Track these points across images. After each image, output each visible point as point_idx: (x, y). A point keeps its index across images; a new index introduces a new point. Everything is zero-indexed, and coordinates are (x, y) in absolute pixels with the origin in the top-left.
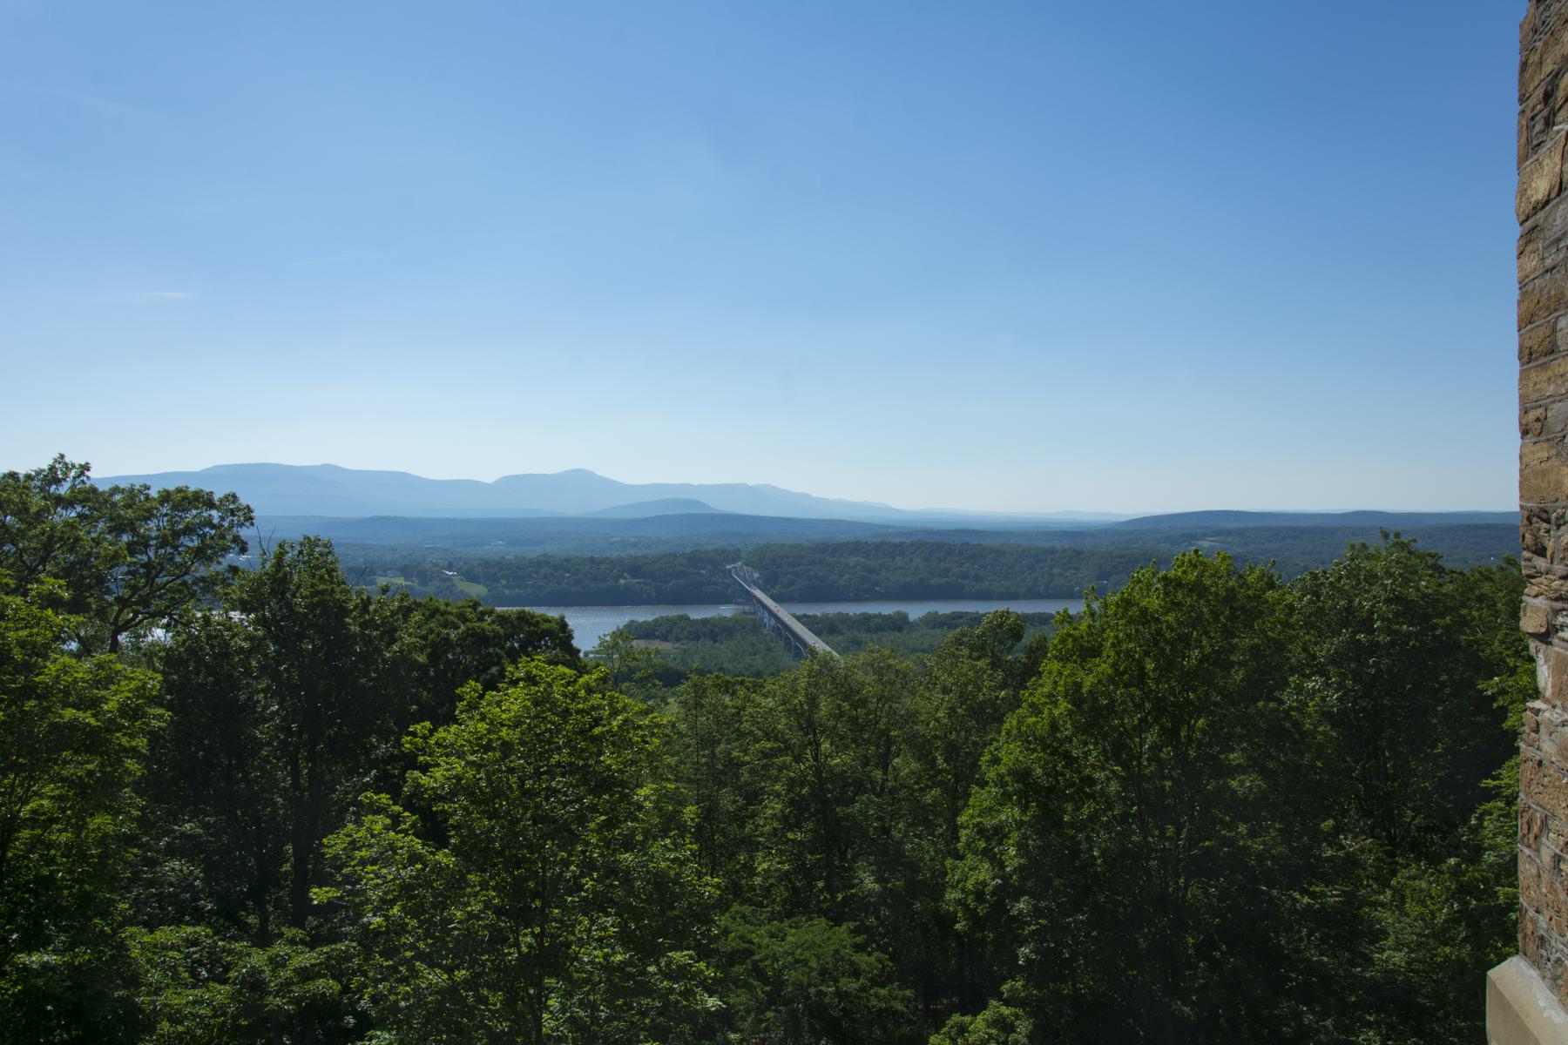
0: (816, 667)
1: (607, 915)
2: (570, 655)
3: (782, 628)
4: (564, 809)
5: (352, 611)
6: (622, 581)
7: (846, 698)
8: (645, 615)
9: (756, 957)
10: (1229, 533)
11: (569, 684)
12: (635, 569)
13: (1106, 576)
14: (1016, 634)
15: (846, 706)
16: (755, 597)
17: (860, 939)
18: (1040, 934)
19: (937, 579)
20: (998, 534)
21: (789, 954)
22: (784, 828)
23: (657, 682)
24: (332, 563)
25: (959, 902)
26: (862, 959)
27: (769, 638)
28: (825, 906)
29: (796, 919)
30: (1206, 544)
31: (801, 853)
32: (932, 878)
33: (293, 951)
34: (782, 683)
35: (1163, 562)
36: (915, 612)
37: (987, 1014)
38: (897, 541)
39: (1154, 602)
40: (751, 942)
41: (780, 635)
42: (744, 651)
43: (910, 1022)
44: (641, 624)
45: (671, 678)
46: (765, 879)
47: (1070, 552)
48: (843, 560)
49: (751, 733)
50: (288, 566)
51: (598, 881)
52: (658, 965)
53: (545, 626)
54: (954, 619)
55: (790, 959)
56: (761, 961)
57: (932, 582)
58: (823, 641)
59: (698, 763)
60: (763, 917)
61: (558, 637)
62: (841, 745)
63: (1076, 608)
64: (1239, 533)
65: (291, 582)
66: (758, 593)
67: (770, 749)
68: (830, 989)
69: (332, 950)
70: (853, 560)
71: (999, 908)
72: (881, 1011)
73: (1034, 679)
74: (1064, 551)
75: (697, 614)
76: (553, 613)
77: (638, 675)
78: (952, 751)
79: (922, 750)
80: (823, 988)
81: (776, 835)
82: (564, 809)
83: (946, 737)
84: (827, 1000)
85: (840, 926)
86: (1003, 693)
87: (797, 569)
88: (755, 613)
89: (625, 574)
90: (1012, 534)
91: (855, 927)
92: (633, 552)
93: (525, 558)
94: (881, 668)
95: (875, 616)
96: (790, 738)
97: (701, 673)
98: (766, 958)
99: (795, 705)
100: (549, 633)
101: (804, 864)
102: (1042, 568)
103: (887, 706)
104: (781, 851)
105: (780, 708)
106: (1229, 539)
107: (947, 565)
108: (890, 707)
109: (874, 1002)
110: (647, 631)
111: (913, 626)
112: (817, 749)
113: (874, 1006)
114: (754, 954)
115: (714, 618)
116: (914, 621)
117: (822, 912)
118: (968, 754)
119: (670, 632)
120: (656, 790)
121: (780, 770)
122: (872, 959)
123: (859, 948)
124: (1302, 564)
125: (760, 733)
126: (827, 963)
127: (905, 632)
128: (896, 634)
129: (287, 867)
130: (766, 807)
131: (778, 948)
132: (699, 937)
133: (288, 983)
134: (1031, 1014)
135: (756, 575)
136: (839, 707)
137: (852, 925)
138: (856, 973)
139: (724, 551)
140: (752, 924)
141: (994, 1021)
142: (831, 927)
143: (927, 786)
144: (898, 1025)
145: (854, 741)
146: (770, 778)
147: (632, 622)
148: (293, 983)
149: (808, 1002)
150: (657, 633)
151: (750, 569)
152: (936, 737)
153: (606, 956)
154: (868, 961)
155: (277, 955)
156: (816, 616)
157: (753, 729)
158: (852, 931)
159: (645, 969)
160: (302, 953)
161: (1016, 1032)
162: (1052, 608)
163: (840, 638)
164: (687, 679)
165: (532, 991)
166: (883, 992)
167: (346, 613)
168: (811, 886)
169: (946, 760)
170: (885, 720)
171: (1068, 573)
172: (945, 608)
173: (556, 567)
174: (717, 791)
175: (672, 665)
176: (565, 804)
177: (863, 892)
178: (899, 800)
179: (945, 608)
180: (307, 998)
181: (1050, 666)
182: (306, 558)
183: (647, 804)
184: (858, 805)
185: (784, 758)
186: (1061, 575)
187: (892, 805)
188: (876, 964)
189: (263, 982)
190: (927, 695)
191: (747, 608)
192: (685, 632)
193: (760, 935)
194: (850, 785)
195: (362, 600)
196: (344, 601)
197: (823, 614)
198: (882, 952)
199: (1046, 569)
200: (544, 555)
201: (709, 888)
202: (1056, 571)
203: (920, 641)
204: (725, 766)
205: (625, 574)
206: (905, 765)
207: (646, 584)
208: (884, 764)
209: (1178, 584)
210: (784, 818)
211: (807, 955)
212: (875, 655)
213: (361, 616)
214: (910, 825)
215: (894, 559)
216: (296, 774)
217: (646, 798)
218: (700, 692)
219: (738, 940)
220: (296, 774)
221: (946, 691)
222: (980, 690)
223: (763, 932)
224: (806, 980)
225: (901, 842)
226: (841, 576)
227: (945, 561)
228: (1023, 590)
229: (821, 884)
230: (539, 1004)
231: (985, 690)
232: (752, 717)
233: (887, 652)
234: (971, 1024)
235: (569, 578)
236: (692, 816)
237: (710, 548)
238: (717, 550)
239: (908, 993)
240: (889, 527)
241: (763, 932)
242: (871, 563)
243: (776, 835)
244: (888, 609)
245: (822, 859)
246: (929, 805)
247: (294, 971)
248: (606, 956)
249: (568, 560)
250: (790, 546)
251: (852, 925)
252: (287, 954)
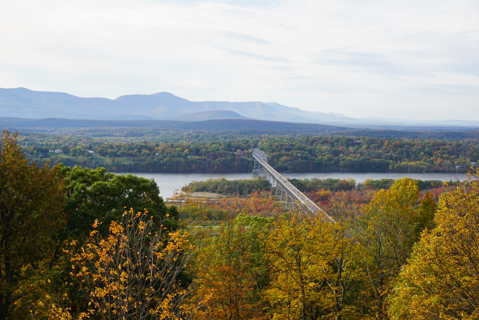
36: (360, 179)
110: (203, 188)
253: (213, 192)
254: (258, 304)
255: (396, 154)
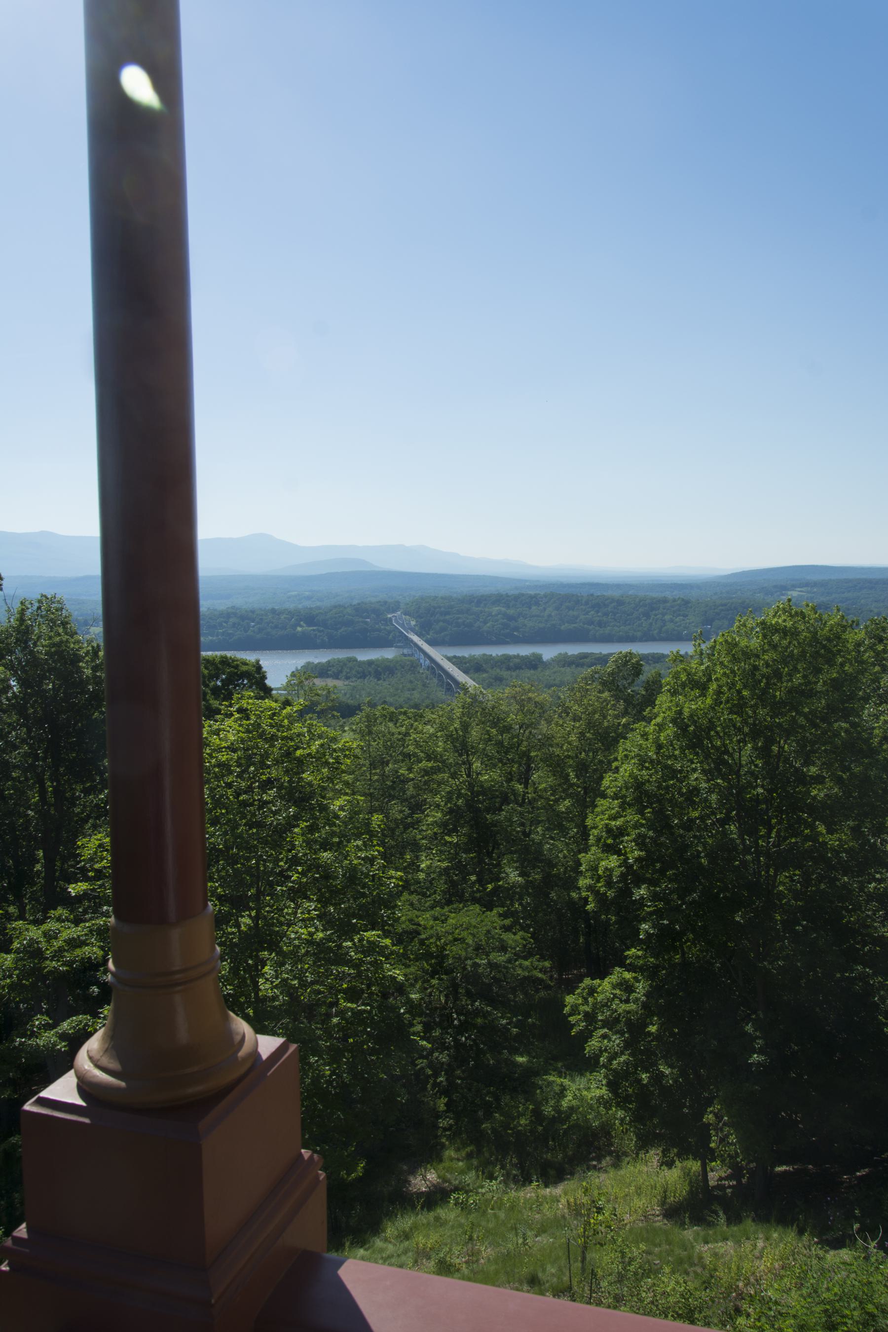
0: (469, 700)
1: (310, 900)
2: (266, 692)
3: (435, 668)
4: (274, 817)
5: (84, 658)
6: (299, 629)
7: (494, 724)
8: (320, 657)
9: (423, 936)
10: (815, 584)
11: (274, 714)
12: (310, 618)
13: (709, 621)
14: (637, 670)
15: (494, 731)
16: (412, 641)
17: (507, 922)
18: (659, 914)
19: (566, 625)
20: (618, 586)
21: (449, 933)
22: (443, 833)
23: (335, 713)
24: (66, 617)
25: (590, 888)
26: (509, 938)
27: (424, 676)
28: (478, 895)
29: (455, 906)
30: (794, 594)
31: (457, 854)
32: (565, 872)
33: (62, 927)
34: (441, 713)
35: (757, 609)
36: (548, 653)
37: (613, 978)
38: (532, 593)
39: (755, 643)
40: (419, 925)
41: (434, 673)
42: (403, 686)
43: (548, 987)
44: (317, 665)
45: (348, 711)
46: (428, 875)
47: (679, 602)
48: (487, 610)
49: (415, 755)
50: (30, 619)
51: (303, 874)
52: (352, 940)
53: (244, 668)
54: (581, 659)
55: (450, 938)
56: (427, 939)
57: (563, 627)
58: (471, 678)
59: (370, 780)
60: (428, 904)
61: (255, 678)
62: (490, 763)
63: (687, 648)
64: (823, 584)
65: (32, 633)
66: (415, 638)
67: (432, 768)
68: (483, 962)
69: (93, 925)
70: (495, 609)
71: (625, 893)
72: (525, 978)
73: (649, 708)
74: (674, 600)
75: (364, 656)
76: (250, 657)
77: (318, 709)
78: (582, 768)
79: (556, 766)
80: (477, 961)
81: (436, 839)
82: (274, 817)
83: (577, 757)
84: (480, 970)
85: (491, 910)
86: (624, 720)
87: (447, 617)
88: (412, 655)
89: (302, 623)
90: (630, 586)
91: (504, 912)
92: (307, 604)
93: (215, 610)
94: (523, 700)
95: (515, 657)
96: (448, 759)
97: (372, 705)
98: (431, 937)
99: (452, 732)
100: (246, 675)
101: (460, 862)
102: (656, 615)
103: (527, 732)
104: (441, 851)
105: (439, 734)
106: (815, 590)
107: (575, 613)
108: (530, 732)
109: (520, 971)
110: (323, 671)
111: (546, 665)
112: (470, 768)
113: (518, 975)
114: (419, 934)
115: (377, 660)
116: (547, 661)
117: (475, 901)
118: (595, 771)
119: (341, 672)
120: (348, 801)
121: (439, 784)
122: (518, 937)
123: (507, 929)
124: (876, 610)
125: (422, 755)
126: (481, 940)
127: (539, 669)
128: (532, 672)
129: (38, 867)
130: (428, 815)
131: (441, 929)
132: (385, 918)
133: (61, 950)
134: (647, 978)
135: (413, 623)
136: (488, 733)
137: (501, 910)
138: (503, 948)
139: (385, 603)
140: (419, 910)
141: (617, 984)
142: (484, 912)
143: (561, 797)
144: (537, 991)
145: (500, 760)
146: (431, 791)
147: (308, 663)
148: (65, 950)
149: (465, 972)
150: (329, 672)
151: (408, 617)
152: (569, 757)
153: (311, 934)
154: (514, 939)
155: (50, 930)
156: (464, 657)
157: (416, 751)
158: (500, 915)
159: (341, 944)
160: (69, 928)
161: (635, 992)
162: (666, 649)
163: (485, 675)
164: (361, 711)
165: (250, 962)
166: (527, 963)
167: (80, 659)
168: (464, 880)
169: (577, 776)
170: (525, 743)
171: (677, 619)
172: (573, 650)
173: (243, 618)
174: (387, 803)
175: (344, 699)
176: (275, 813)
177: (509, 884)
178: (538, 809)
179: (573, 650)
180: (77, 961)
181: (663, 700)
182: (44, 613)
183: (342, 814)
184: (504, 813)
185: (442, 775)
186: (672, 621)
187: (532, 813)
188: (521, 941)
189: (40, 949)
190: (561, 722)
191: (406, 651)
192: (354, 672)
193: (425, 919)
194: (498, 797)
195: (93, 647)
196: (77, 650)
197: (470, 655)
198: (525, 932)
199: (659, 616)
200: (233, 607)
201: (394, 880)
202: (667, 617)
203: (553, 678)
204: (394, 782)
205: (302, 623)
206: (542, 779)
207: (320, 631)
208: (525, 779)
209: (776, 629)
210: (444, 825)
211: (464, 934)
212: (518, 689)
213: (93, 660)
214: (548, 829)
215: (530, 608)
216: (43, 792)
217: (341, 808)
218: (371, 721)
219: (407, 922)
220: (43, 792)
221: (576, 719)
222: (605, 717)
223: (428, 916)
224: (463, 954)
225: (540, 844)
226: (485, 622)
227: (573, 610)
228: (639, 634)
229: (473, 878)
230: (256, 972)
231: (609, 717)
232: (416, 741)
233: (527, 687)
234: (599, 986)
235: (253, 627)
236: (378, 823)
237: (373, 600)
238: (380, 602)
239: (547, 964)
240: (526, 581)
241: (428, 916)
242: (511, 612)
243: (436, 839)
244: (525, 651)
245: (475, 857)
246: (563, 812)
247: (65, 941)
248: (311, 934)
249: (253, 612)
250: (442, 598)
251: (501, 910)
252: (58, 929)
253: (337, 678)
254: (410, 876)
255: (598, 616)
